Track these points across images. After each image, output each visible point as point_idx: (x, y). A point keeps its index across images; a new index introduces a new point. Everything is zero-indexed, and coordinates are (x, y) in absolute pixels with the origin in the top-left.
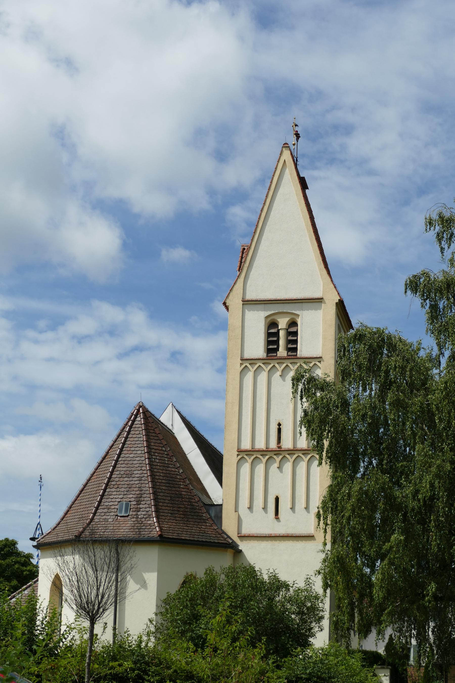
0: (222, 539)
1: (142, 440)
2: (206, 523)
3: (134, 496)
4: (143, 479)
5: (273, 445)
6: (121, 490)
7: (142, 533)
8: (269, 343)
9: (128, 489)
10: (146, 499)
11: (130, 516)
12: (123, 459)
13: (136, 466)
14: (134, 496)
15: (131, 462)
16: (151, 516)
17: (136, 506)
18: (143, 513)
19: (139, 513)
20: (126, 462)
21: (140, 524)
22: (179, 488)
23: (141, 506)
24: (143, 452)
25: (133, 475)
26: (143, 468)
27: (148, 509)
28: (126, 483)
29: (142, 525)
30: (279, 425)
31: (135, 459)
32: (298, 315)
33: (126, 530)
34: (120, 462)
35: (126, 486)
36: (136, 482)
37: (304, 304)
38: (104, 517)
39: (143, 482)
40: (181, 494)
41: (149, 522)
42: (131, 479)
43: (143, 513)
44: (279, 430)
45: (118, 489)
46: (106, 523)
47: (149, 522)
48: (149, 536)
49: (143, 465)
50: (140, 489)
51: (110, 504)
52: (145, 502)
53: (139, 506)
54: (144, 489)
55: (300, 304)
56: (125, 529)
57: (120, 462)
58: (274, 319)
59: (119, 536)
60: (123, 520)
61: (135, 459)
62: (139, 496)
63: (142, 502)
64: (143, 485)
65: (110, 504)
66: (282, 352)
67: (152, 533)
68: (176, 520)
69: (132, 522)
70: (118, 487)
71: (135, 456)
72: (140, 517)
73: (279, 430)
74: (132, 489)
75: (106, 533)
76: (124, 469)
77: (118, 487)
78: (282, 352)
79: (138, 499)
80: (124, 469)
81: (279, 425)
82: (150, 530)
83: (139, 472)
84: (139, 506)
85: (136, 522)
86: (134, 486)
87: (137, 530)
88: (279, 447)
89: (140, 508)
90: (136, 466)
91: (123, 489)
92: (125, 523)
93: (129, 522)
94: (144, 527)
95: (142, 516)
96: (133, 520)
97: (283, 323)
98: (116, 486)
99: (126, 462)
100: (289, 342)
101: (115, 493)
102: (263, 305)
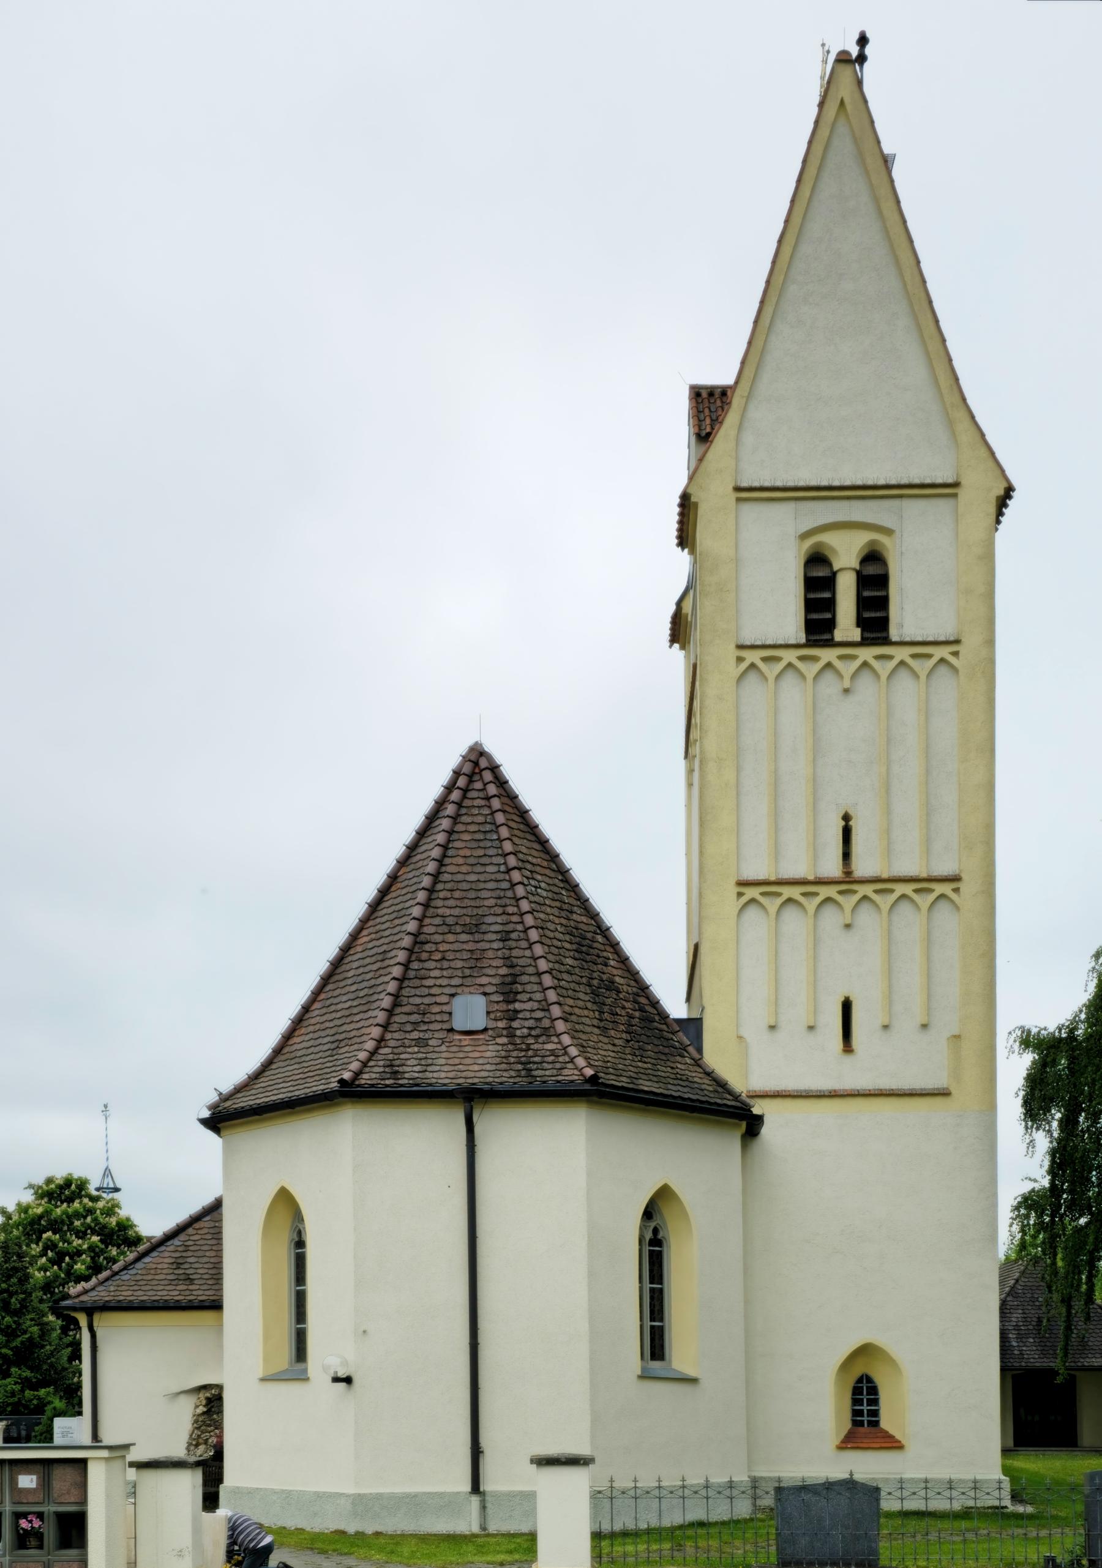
0: (729, 1097)
1: (495, 837)
2: (684, 1057)
3: (495, 981)
4: (514, 936)
5: (832, 867)
6: (452, 964)
7: (535, 1073)
8: (811, 605)
9: (472, 963)
10: (528, 988)
11: (490, 1032)
12: (449, 886)
13: (487, 903)
14: (495, 981)
15: (472, 894)
16: (552, 1032)
17: (504, 1007)
18: (528, 1024)
19: (515, 1024)
20: (457, 894)
21: (522, 1050)
22: (606, 965)
23: (517, 1006)
24: (503, 868)
25: (484, 928)
26: (510, 910)
27: (539, 1014)
28: (465, 946)
29: (530, 1053)
30: (846, 818)
31: (482, 886)
32: (888, 532)
33: (488, 1067)
34: (442, 895)
35: (466, 955)
36: (495, 945)
37: (906, 503)
38: (415, 1035)
39: (513, 944)
40: (613, 982)
41: (550, 1046)
42: (477, 937)
43: (528, 1024)
44: (847, 833)
45: (445, 964)
46: (422, 1050)
47: (550, 1046)
48: (558, 1082)
49: (508, 902)
50: (508, 963)
51: (427, 1000)
52: (528, 996)
53: (511, 1007)
54: (521, 962)
55: (896, 503)
56: (482, 1065)
57: (442, 895)
58: (820, 544)
59: (470, 1081)
60: (472, 1043)
61: (482, 886)
62: (509, 979)
63: (519, 997)
64: (515, 953)
65: (427, 1000)
66: (846, 626)
67: (565, 1072)
68: (614, 1045)
69: (500, 1048)
70: (443, 959)
71: (482, 877)
72: (518, 1033)
73: (847, 833)
74: (485, 963)
75: (428, 1075)
76: (457, 912)
77: (443, 959)
78: (846, 626)
79: (507, 989)
80: (457, 912)
81: (846, 818)
82: (558, 1066)
83: (499, 919)
84: (511, 1007)
85: (510, 1047)
86: (490, 954)
87: (520, 1067)
88: (848, 873)
89: (516, 1011)
90: (487, 903)
91: (459, 964)
92: (480, 1048)
93: (490, 1048)
94: (537, 1059)
95: (525, 1031)
96: (500, 1040)
97: (846, 555)
98: (438, 956)
99: (457, 894)
100: (863, 604)
101: (436, 973)
102: (792, 505)
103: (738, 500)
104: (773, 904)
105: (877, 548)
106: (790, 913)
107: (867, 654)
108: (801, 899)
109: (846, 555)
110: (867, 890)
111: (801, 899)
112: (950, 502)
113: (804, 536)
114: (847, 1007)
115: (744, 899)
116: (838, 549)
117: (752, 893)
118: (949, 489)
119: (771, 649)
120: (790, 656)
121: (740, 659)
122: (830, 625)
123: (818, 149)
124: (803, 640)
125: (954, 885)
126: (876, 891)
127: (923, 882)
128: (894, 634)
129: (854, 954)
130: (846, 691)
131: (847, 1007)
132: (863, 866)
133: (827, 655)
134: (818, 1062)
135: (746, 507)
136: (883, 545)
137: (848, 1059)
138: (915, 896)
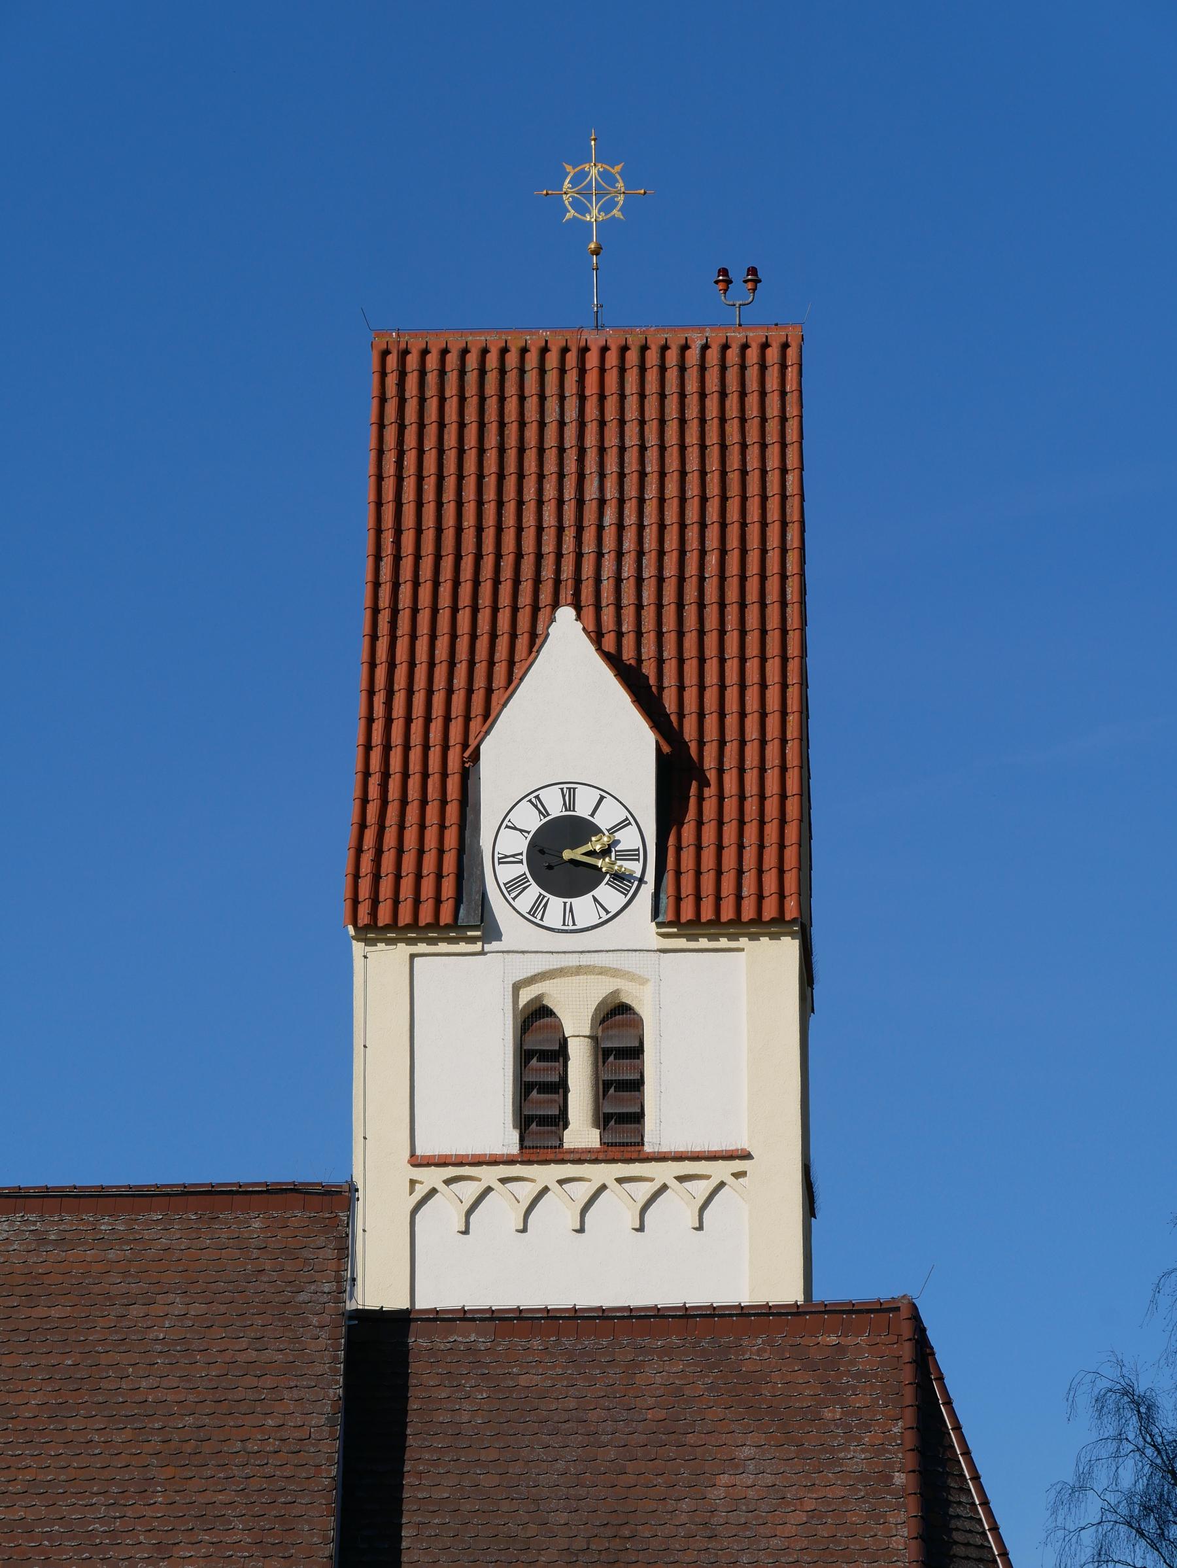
66: (581, 1131)
78: (581, 1131)
97: (576, 1022)
109: (576, 1022)
122: (561, 1120)
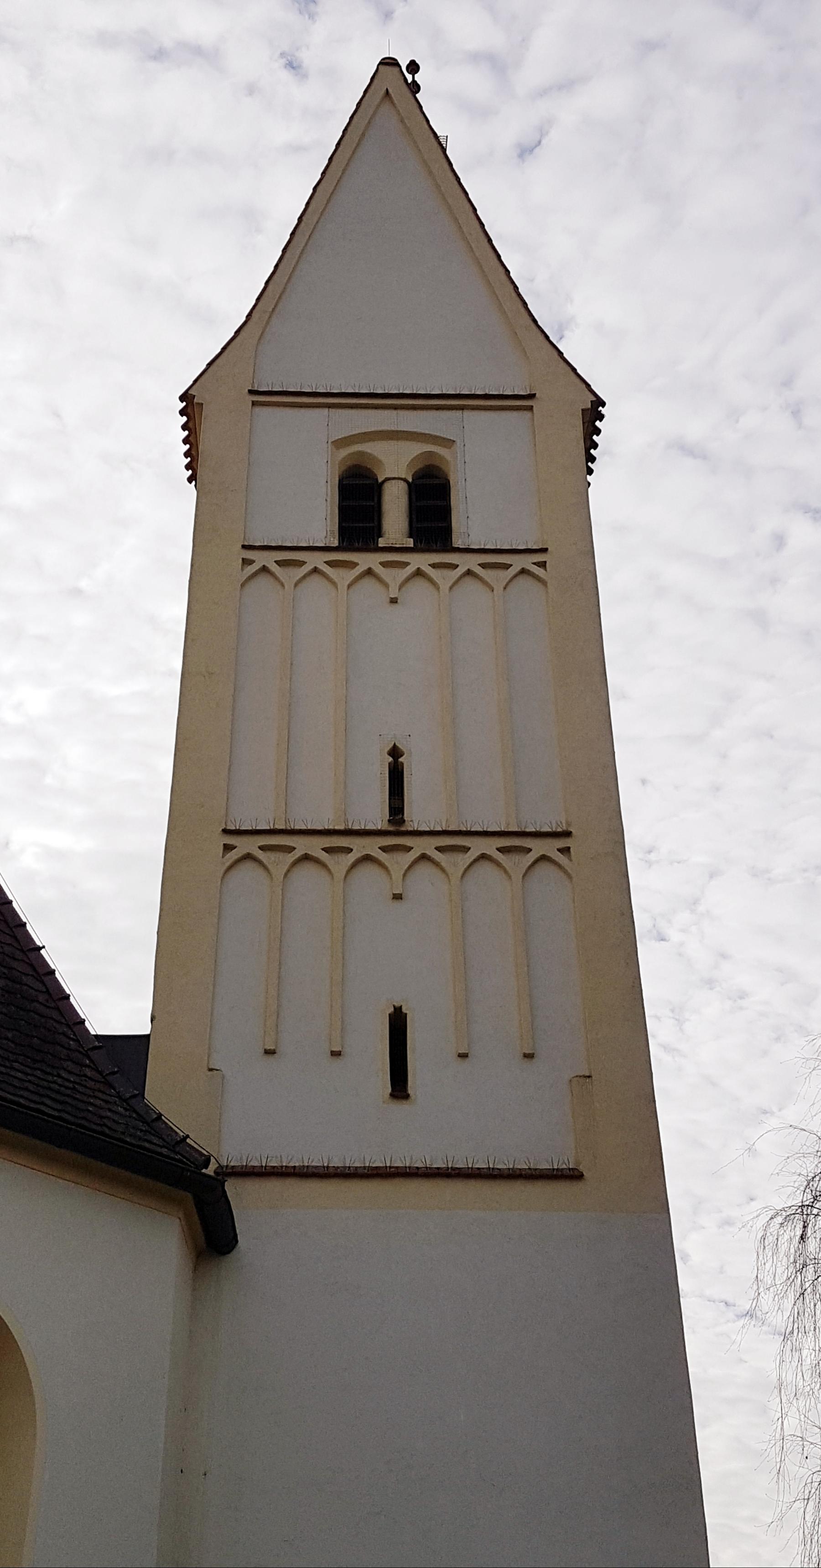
5: (375, 814)
30: (395, 752)
32: (448, 443)
58: (361, 454)
97: (395, 464)
103: (254, 404)
104: (279, 863)
105: (437, 463)
106: (307, 873)
107: (421, 561)
108: (324, 856)
109: (395, 464)
110: (427, 846)
111: (324, 856)
112: (527, 415)
113: (340, 443)
114: (398, 1024)
115: (233, 855)
116: (381, 457)
117: (245, 845)
118: (523, 402)
119: (289, 554)
120: (317, 560)
121: (246, 562)
123: (354, 135)
124: (335, 543)
125: (561, 843)
126: (384, 849)
127: (514, 839)
128: (457, 542)
129: (403, 938)
130: (394, 601)
131: (398, 1024)
132: (417, 814)
133: (366, 560)
134: (350, 1118)
135: (258, 410)
136: (442, 458)
137: (400, 1108)
138: (383, 857)
